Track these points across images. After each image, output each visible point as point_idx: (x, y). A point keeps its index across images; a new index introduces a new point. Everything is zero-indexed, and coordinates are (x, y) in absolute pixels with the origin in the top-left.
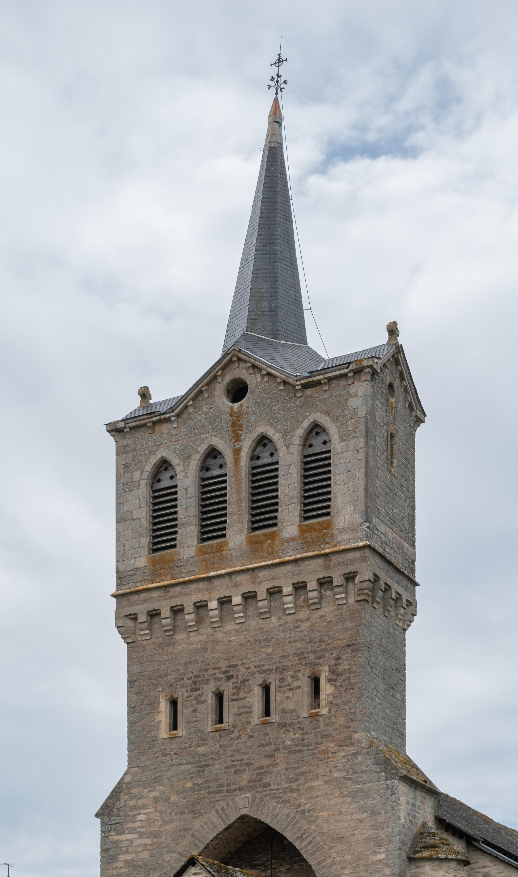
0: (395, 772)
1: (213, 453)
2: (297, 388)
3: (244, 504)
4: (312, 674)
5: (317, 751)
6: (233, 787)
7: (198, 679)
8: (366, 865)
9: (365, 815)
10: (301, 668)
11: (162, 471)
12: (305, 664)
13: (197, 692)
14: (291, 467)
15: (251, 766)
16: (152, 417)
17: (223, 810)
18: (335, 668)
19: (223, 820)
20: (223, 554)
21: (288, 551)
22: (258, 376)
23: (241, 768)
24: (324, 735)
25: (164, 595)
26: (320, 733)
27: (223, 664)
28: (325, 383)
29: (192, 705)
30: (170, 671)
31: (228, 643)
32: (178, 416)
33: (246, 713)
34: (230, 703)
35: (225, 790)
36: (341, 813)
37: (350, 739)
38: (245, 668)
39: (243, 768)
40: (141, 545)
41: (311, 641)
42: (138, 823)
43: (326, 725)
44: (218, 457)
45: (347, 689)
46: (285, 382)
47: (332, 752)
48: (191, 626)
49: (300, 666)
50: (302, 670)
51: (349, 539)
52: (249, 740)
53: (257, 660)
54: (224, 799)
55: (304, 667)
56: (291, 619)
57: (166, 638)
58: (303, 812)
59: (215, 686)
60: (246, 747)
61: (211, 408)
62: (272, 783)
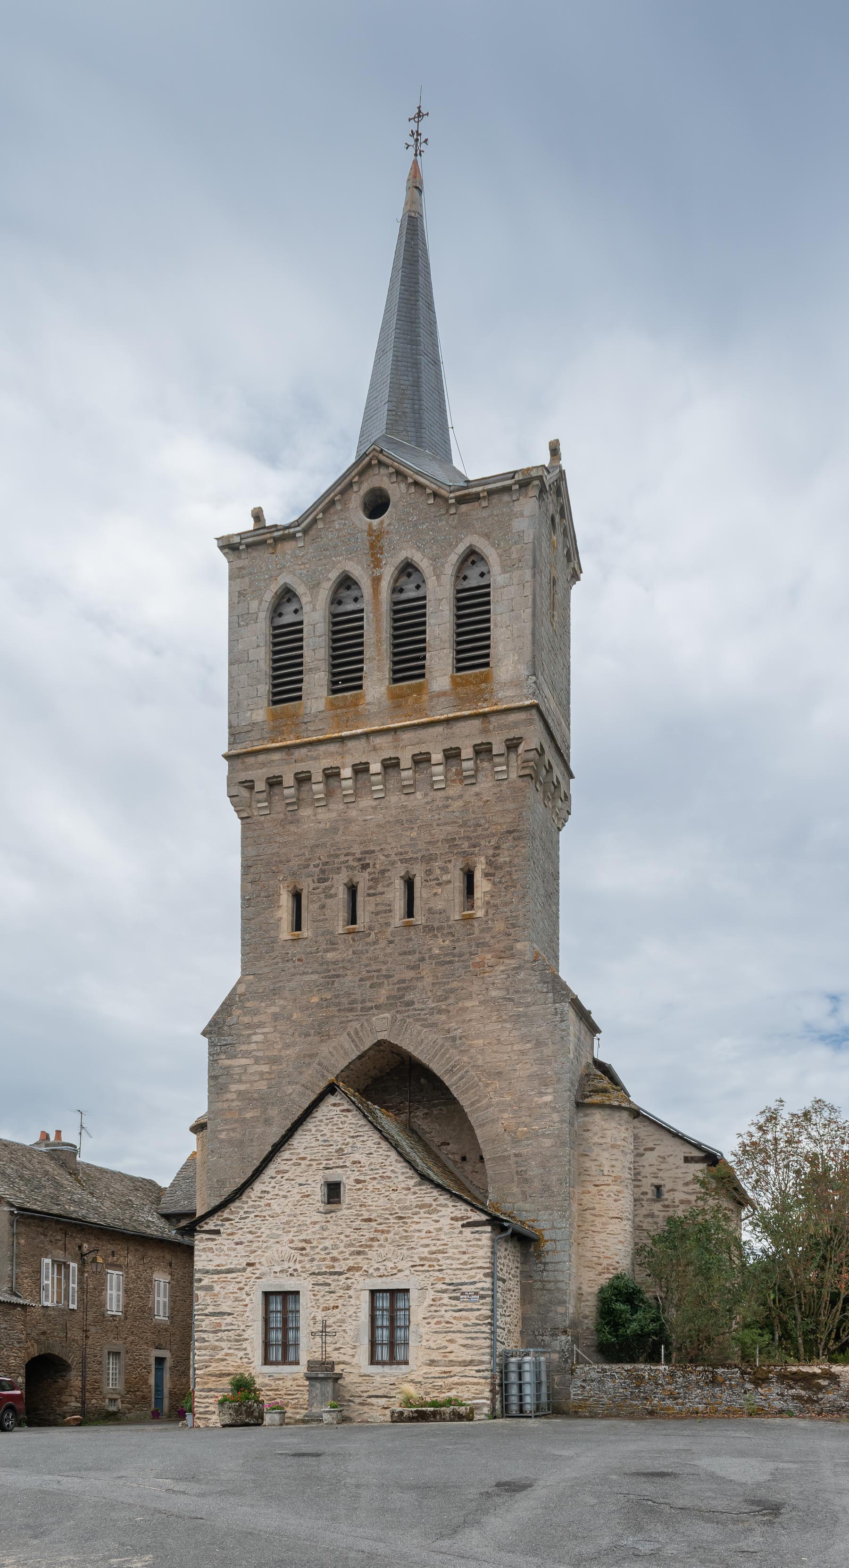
1: (346, 582)
5: (471, 963)
6: (369, 1004)
8: (529, 1109)
9: (529, 1045)
13: (326, 884)
14: (442, 603)
17: (357, 1033)
18: (493, 859)
19: (356, 1046)
22: (403, 486)
27: (357, 850)
28: (484, 497)
30: (292, 855)
31: (364, 823)
32: (305, 531)
33: (385, 912)
36: (499, 1042)
41: (464, 824)
44: (353, 587)
46: (435, 495)
48: (319, 800)
51: (513, 697)
58: (454, 1039)
61: (345, 524)
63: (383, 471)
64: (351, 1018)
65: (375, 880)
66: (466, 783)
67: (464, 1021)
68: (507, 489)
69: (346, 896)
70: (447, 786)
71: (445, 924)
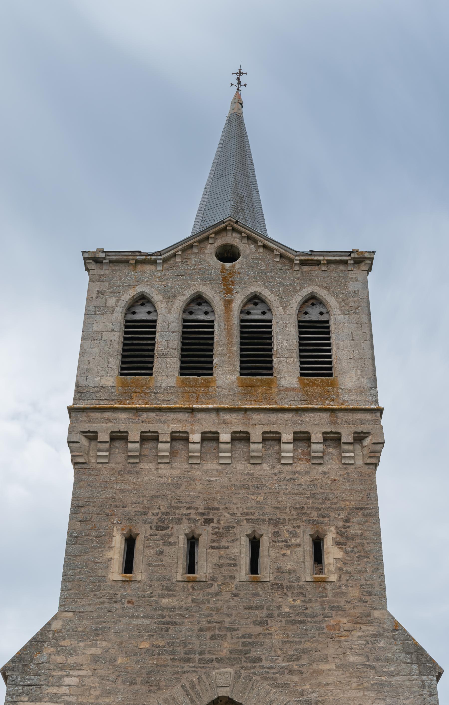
0: (431, 665)
2: (295, 262)
3: (235, 348)
4: (315, 533)
6: (210, 657)
7: (166, 517)
10: (300, 524)
11: (138, 305)
12: (306, 521)
13: (165, 532)
14: (289, 325)
15: (235, 632)
16: (137, 256)
17: (193, 686)
20: (210, 390)
21: (287, 399)
22: (253, 247)
23: (220, 633)
24: (333, 606)
25: (134, 418)
26: (328, 603)
27: (200, 505)
28: (324, 264)
29: (157, 546)
30: (130, 502)
31: (208, 483)
32: (165, 261)
33: (230, 565)
34: (209, 551)
35: (197, 659)
37: (367, 616)
38: (228, 513)
39: (223, 633)
40: (110, 365)
41: (312, 496)
42: (64, 688)
43: (336, 595)
44: (203, 304)
45: (361, 556)
47: (345, 629)
48: (163, 457)
49: (299, 521)
50: (302, 526)
51: (358, 401)
52: (233, 599)
53: (245, 507)
54: (194, 671)
55: (304, 524)
56: (287, 469)
57: (129, 466)
59: (190, 527)
60: (229, 607)
61: (200, 262)
62: (264, 659)
63: (235, 235)
64: (186, 669)
65: (219, 535)
66: (313, 462)
67: (319, 685)
68: (345, 262)
69: (186, 546)
70: (294, 462)
71: (296, 584)
